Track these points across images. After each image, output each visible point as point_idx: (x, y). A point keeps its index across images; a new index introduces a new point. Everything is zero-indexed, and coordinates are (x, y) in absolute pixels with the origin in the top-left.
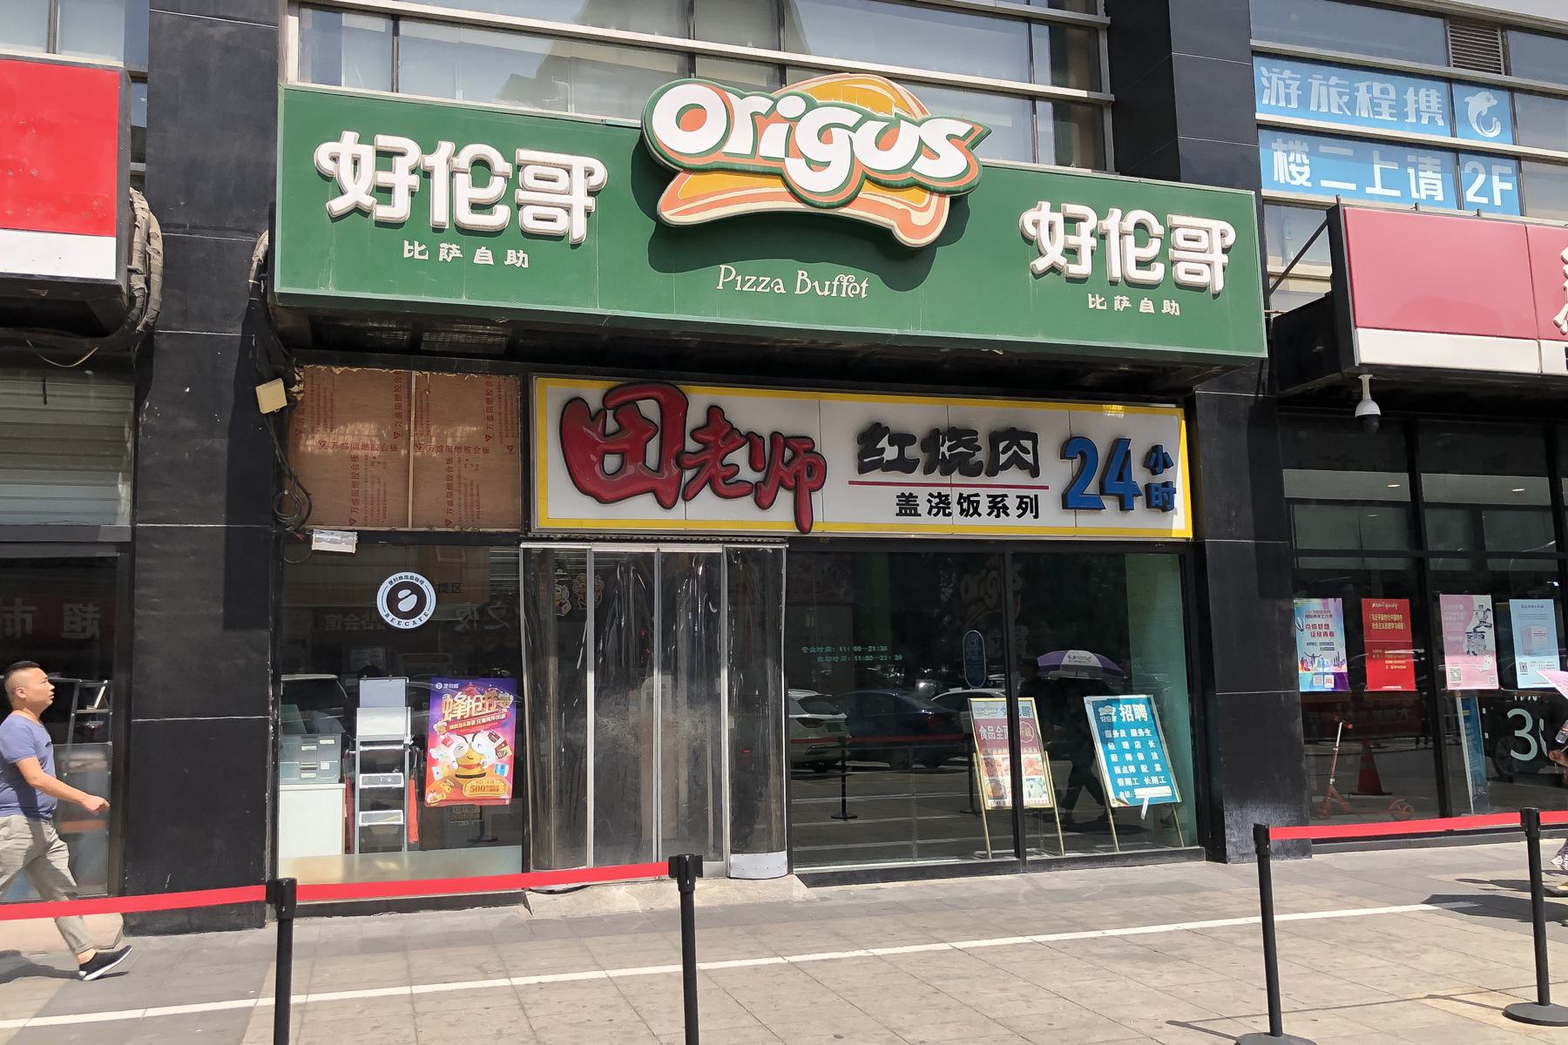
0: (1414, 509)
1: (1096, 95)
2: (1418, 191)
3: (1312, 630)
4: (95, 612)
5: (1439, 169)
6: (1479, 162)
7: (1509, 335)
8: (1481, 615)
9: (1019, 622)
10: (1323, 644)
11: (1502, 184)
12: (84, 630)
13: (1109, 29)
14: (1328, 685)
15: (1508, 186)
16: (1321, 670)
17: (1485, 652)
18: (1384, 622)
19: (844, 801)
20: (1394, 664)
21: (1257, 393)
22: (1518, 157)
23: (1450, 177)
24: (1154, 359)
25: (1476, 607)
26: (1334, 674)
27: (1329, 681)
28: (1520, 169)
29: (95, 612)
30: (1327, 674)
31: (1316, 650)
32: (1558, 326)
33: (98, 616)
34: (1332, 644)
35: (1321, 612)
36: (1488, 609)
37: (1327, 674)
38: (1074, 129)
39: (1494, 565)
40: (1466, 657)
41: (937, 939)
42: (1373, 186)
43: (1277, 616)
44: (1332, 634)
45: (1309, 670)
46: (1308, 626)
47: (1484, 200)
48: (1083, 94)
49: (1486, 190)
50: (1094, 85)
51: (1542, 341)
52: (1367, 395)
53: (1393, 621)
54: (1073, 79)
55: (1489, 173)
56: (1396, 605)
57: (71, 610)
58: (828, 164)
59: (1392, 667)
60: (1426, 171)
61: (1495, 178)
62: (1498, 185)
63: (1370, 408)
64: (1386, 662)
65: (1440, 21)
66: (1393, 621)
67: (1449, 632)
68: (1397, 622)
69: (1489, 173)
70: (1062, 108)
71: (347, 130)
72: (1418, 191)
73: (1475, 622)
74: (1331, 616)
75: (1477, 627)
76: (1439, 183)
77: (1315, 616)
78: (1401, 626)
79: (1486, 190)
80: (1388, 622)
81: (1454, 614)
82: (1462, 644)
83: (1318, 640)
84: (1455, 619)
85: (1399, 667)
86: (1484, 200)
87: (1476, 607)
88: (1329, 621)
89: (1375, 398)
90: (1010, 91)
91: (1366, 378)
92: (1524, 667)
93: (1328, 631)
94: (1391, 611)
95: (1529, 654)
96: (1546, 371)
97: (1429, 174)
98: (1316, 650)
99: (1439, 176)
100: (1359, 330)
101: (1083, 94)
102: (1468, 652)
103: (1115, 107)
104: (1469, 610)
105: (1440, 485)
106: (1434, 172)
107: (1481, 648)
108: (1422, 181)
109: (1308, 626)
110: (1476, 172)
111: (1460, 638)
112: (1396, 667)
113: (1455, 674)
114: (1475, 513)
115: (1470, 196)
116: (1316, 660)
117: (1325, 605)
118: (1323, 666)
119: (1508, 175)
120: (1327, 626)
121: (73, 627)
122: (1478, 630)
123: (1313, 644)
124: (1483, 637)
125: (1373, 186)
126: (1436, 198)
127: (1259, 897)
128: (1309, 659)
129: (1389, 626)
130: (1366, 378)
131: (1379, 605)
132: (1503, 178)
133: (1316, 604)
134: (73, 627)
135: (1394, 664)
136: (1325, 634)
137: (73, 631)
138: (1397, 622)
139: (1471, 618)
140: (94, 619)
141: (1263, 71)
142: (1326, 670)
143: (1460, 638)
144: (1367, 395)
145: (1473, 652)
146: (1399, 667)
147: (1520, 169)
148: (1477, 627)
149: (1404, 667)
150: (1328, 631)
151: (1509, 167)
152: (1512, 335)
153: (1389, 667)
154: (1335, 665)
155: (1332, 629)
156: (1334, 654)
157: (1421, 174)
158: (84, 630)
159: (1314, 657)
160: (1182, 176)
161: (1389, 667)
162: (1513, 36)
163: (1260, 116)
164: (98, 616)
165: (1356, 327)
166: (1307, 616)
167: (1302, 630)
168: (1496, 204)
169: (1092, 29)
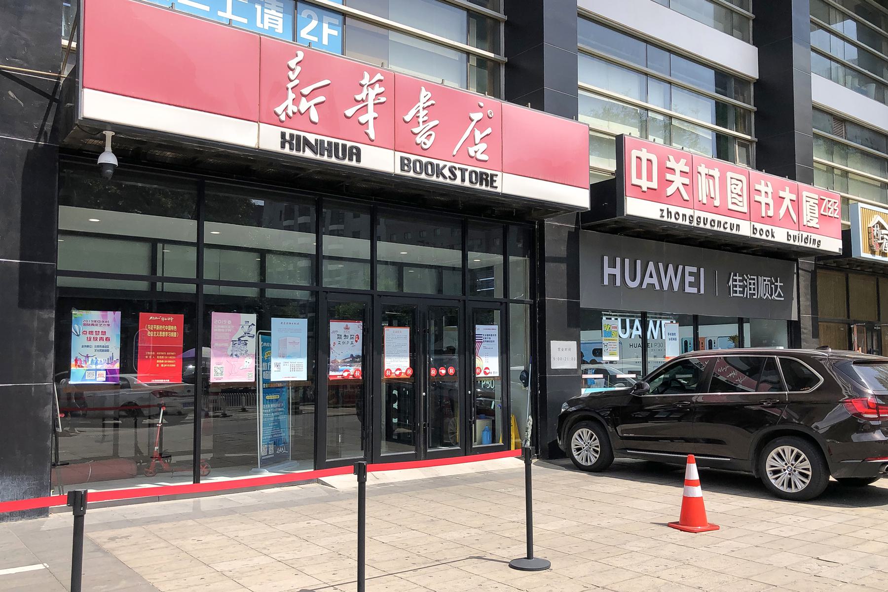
0: (317, 259)
1: (498, 57)
2: (262, 22)
3: (88, 336)
5: (282, 10)
6: (314, 11)
7: (238, 116)
8: (246, 328)
10: (98, 346)
11: (329, 31)
13: (507, 23)
14: (101, 379)
15: (335, 33)
16: (94, 367)
17: (246, 354)
18: (159, 331)
20: (164, 363)
21: (38, 140)
22: (344, 14)
23: (290, 17)
25: (243, 323)
26: (106, 370)
27: (100, 375)
28: (344, 23)
30: (100, 370)
31: (90, 351)
32: (278, 115)
34: (108, 347)
35: (99, 321)
36: (253, 324)
37: (100, 370)
38: (486, 72)
39: (270, 293)
40: (230, 358)
42: (224, 10)
43: (36, 324)
44: (108, 339)
45: (82, 367)
46: (85, 333)
47: (315, 39)
48: (492, 55)
49: (317, 32)
51: (261, 124)
52: (108, 148)
53: (167, 331)
54: (487, 45)
55: (321, 21)
56: (172, 319)
59: (162, 365)
60: (271, 10)
61: (325, 26)
62: (326, 30)
63: (108, 158)
64: (158, 361)
66: (167, 331)
67: (216, 340)
68: (171, 331)
69: (321, 21)
70: (482, 61)
72: (262, 22)
73: (240, 333)
74: (109, 325)
75: (242, 337)
76: (281, 21)
77: (93, 325)
78: (174, 335)
79: (317, 32)
80: (162, 331)
81: (222, 327)
82: (227, 349)
83: (93, 343)
84: (223, 330)
85: (168, 365)
86: (315, 39)
87: (243, 323)
88: (106, 329)
89: (115, 151)
90: (321, 5)
91: (109, 134)
92: (278, 365)
93: (105, 337)
94: (167, 323)
95: (283, 357)
96: (504, 192)
97: (273, 12)
98: (90, 351)
99: (281, 15)
100: (86, 90)
101: (492, 55)
102: (232, 355)
103: (507, 65)
104: (237, 324)
105: (387, 250)
106: (277, 11)
107: (243, 352)
108: (266, 17)
109: (85, 333)
110: (310, 17)
111: (226, 345)
112: (166, 365)
113: (219, 371)
114: (400, 267)
115: (304, 33)
116: (90, 359)
117: (104, 317)
118: (96, 364)
119: (335, 25)
120: (104, 333)
122: (242, 339)
123: (88, 346)
124: (246, 344)
125: (224, 10)
126: (276, 30)
127: (356, 530)
128: (83, 359)
129: (163, 334)
130: (109, 134)
131: (156, 318)
132: (331, 26)
133: (95, 315)
135: (164, 363)
136: (101, 339)
138: (171, 331)
139: (237, 330)
142: (99, 367)
143: (226, 345)
144: (108, 148)
145: (236, 355)
146: (168, 365)
147: (344, 23)
148: (242, 337)
149: (174, 365)
150: (105, 337)
151: (337, 20)
152: (240, 117)
153: (160, 365)
154: (108, 364)
155: (107, 335)
156: (109, 355)
157: (266, 11)
159: (87, 357)
161: (160, 365)
165: (83, 87)
166: (85, 325)
167: (78, 335)
168: (323, 43)
169: (496, 21)
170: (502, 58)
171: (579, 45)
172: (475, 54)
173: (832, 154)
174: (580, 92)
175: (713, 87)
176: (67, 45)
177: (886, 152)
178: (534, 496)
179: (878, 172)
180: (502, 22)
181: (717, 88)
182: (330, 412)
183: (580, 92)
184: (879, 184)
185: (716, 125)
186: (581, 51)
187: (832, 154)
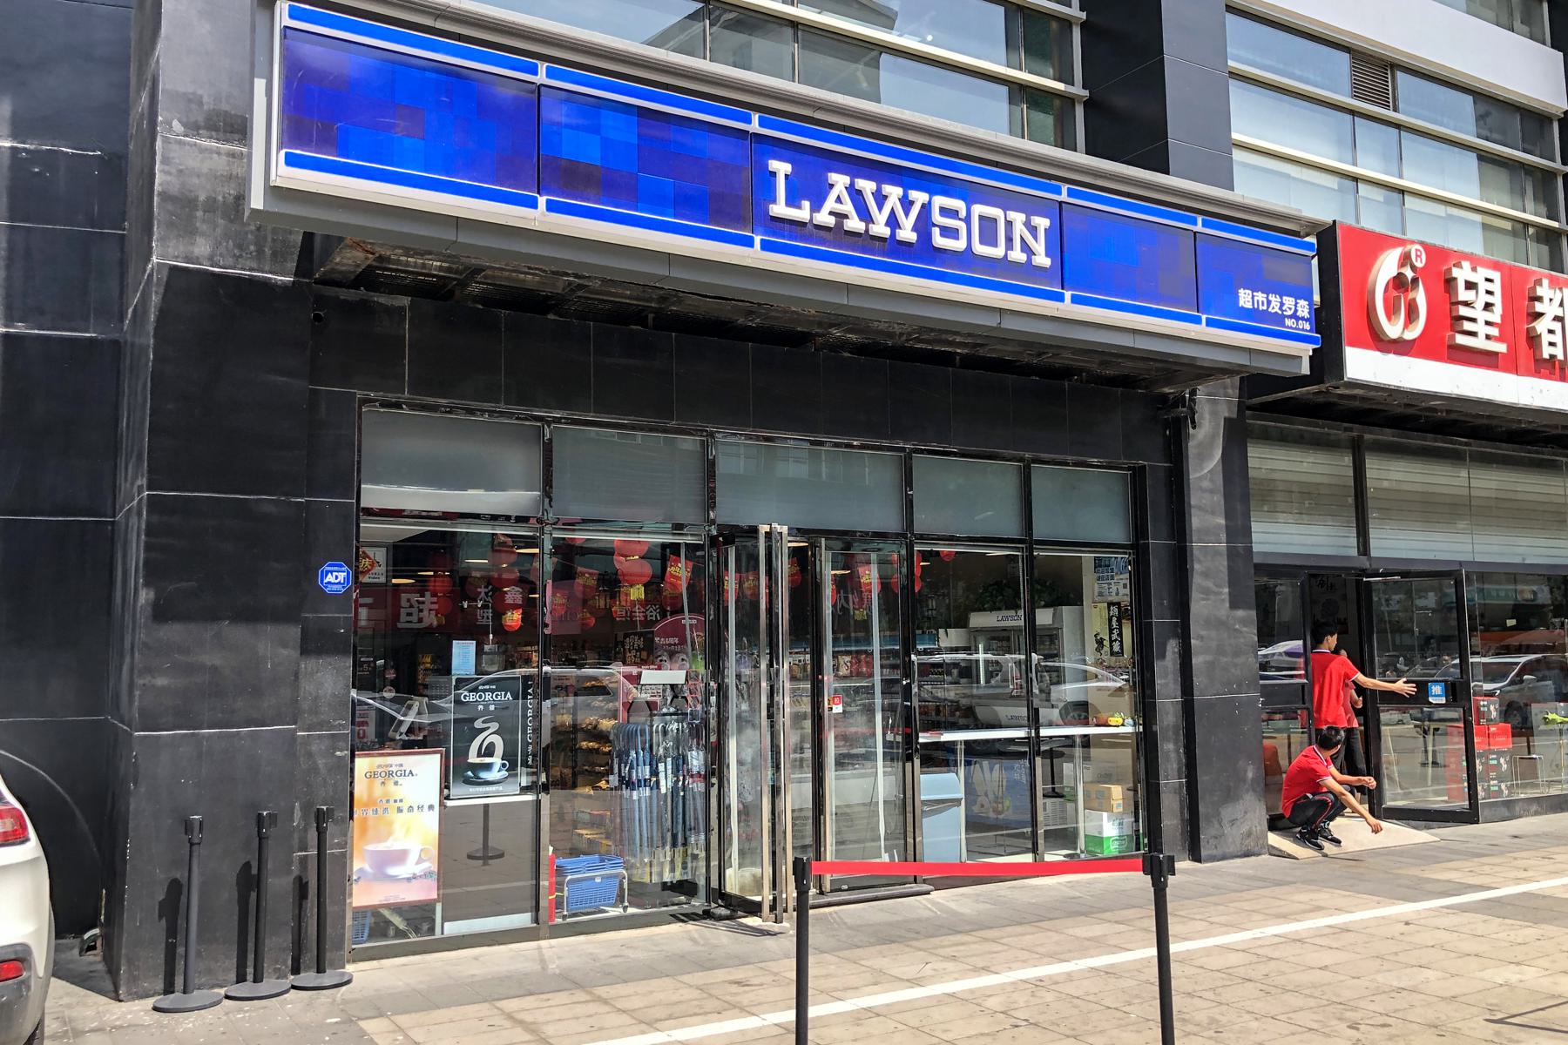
1: (1071, 89)
4: (432, 603)
9: (551, 554)
12: (420, 620)
19: (1053, 783)
24: (1466, 409)
29: (432, 603)
33: (436, 606)
41: (1430, 892)
48: (1060, 86)
50: (1065, 76)
57: (409, 600)
58: (1554, 319)
65: (1346, 56)
71: (976, 203)
90: (764, 11)
101: (1060, 86)
121: (409, 618)
134: (409, 618)
137: (411, 622)
140: (430, 610)
141: (1238, 96)
158: (420, 620)
160: (754, 63)
162: (1400, 75)
163: (1235, 136)
164: (436, 606)
170: (1077, 90)
171: (1231, 63)
172: (1534, 225)
173: (1523, 194)
174: (1238, 155)
175: (1347, 87)
176: (256, 80)
177: (1538, 152)
178: (812, 983)
179: (1506, 198)
180: (1077, 24)
181: (1480, 131)
182: (923, 777)
183: (1238, 155)
184: (1508, 225)
185: (1482, 200)
186: (1235, 75)
187: (1523, 194)
